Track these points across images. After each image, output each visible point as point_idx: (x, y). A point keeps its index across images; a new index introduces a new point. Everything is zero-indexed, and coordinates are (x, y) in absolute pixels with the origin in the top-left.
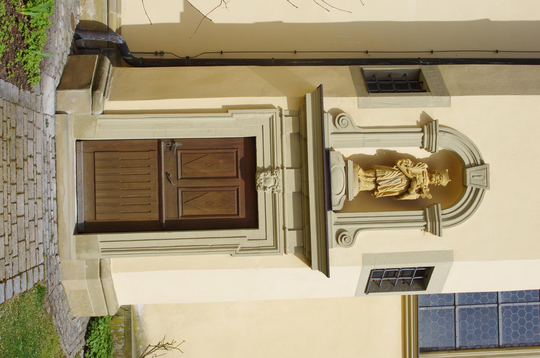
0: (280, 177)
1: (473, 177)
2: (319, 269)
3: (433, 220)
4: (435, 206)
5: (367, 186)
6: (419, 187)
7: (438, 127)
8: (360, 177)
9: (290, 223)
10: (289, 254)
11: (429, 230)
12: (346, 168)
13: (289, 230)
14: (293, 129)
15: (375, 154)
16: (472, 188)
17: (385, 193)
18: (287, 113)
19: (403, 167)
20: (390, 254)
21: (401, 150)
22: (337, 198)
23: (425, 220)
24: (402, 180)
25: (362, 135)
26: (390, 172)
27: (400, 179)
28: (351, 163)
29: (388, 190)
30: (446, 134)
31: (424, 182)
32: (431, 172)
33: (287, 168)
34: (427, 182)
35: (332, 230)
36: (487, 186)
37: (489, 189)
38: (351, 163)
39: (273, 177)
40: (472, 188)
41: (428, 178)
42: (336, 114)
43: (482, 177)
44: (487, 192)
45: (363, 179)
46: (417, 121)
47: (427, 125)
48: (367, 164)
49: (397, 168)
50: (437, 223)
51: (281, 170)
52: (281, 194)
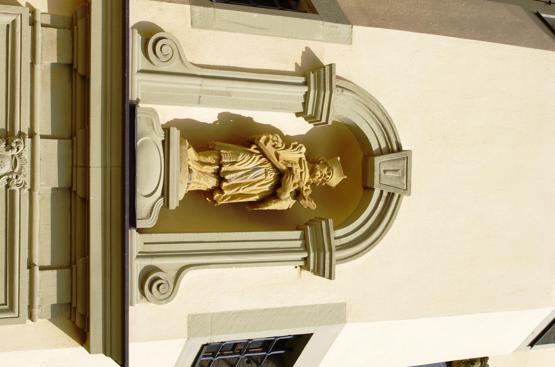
0: (27, 155)
1: (385, 171)
2: (105, 353)
3: (320, 249)
4: (323, 223)
5: (202, 181)
6: (297, 187)
7: (334, 77)
8: (190, 163)
9: (43, 254)
10: (38, 321)
11: (312, 268)
12: (166, 144)
13: (42, 268)
14: (59, 55)
15: (215, 122)
16: (382, 192)
17: (233, 197)
18: (47, 20)
19: (269, 149)
20: (240, 314)
21: (261, 117)
22: (147, 203)
23: (306, 247)
24: (266, 173)
25: (198, 81)
26: (247, 157)
27: (262, 171)
28: (175, 134)
29: (241, 191)
30: (345, 92)
31: (302, 177)
32: (313, 161)
33: (42, 137)
34: (307, 177)
35: (136, 267)
36: (407, 189)
37: (410, 195)
38: (175, 134)
39: (10, 153)
40: (382, 192)
41: (307, 170)
42: (149, 32)
43: (399, 174)
44: (405, 199)
45: (195, 167)
46: (297, 65)
47: (315, 74)
48: (203, 140)
49: (258, 149)
50: (327, 255)
51: (28, 141)
52: (26, 192)
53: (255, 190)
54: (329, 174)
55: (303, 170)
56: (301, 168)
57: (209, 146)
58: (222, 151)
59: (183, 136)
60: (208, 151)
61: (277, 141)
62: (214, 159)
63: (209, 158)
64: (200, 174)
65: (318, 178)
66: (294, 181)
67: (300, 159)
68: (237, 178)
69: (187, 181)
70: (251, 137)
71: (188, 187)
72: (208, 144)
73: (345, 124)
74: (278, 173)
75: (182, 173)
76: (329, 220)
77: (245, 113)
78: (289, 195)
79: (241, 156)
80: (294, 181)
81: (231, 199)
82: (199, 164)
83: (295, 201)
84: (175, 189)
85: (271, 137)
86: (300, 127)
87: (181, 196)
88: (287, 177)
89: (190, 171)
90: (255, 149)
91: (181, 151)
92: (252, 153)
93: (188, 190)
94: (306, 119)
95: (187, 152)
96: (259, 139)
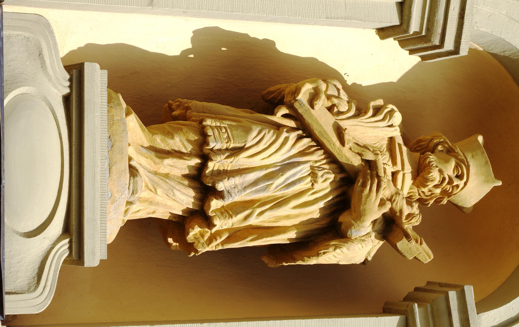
4: (453, 295)
5: (160, 197)
6: (386, 209)
8: (131, 151)
12: (74, 104)
17: (235, 234)
19: (320, 118)
21: (293, 40)
26: (269, 136)
27: (304, 170)
28: (96, 80)
29: (254, 221)
32: (419, 147)
34: (407, 184)
41: (408, 169)
45: (143, 162)
48: (160, 96)
53: (288, 217)
54: (459, 177)
55: (399, 167)
56: (394, 163)
57: (172, 110)
58: (208, 122)
59: (114, 85)
60: (172, 123)
61: (338, 97)
62: (189, 141)
63: (177, 139)
64: (156, 179)
65: (432, 189)
66: (380, 196)
67: (391, 140)
68: (245, 188)
69: (126, 196)
70: (272, 89)
71: (126, 211)
72: (170, 106)
73: (494, 55)
74: (339, 176)
75: (114, 176)
76: (466, 288)
77: (257, 30)
78: (369, 229)
79: (254, 133)
80: (380, 196)
81: (228, 240)
82: (152, 154)
83: (382, 243)
84: (98, 217)
85: (323, 86)
86: (388, 64)
87: (112, 235)
88: (364, 185)
89: (133, 171)
90: (285, 116)
91: (111, 122)
92: (278, 127)
93: (126, 219)
94: (403, 43)
95: (125, 124)
96: (297, 91)
